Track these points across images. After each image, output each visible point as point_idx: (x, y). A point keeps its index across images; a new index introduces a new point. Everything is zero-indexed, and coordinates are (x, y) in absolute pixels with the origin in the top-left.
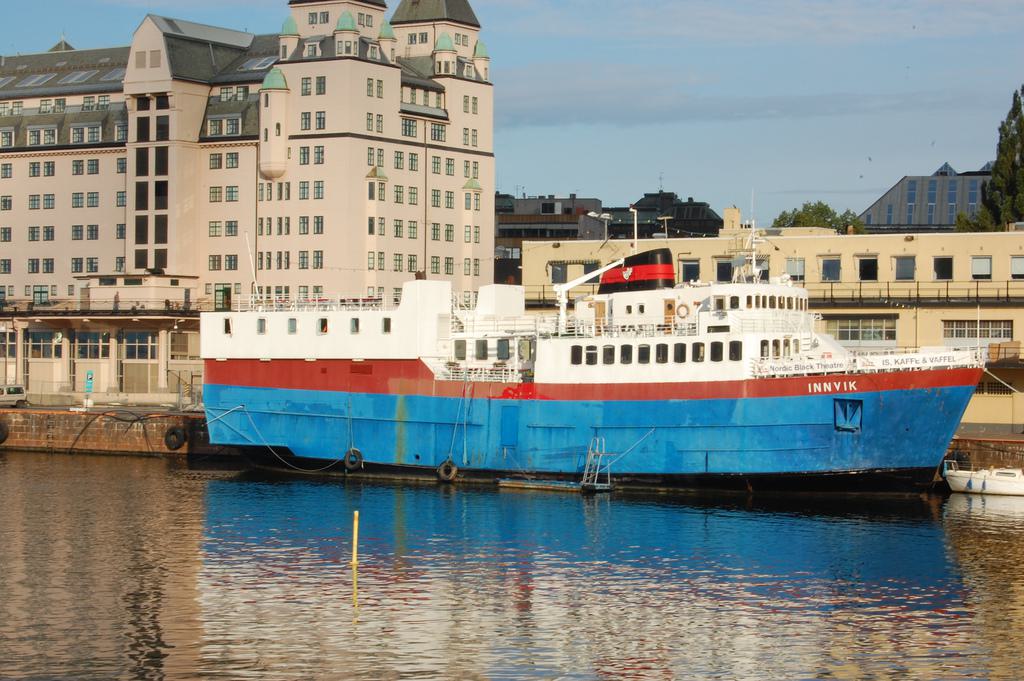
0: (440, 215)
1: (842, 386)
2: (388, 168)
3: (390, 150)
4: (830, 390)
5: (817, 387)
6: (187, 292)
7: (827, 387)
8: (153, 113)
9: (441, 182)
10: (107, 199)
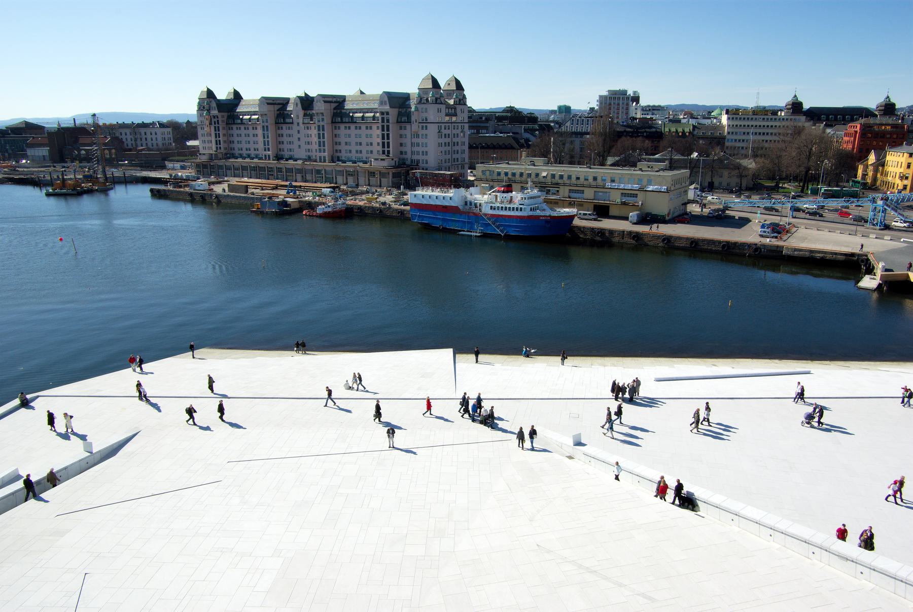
0: (455, 140)
2: (443, 130)
3: (443, 125)
8: (385, 116)
9: (455, 132)
10: (375, 136)
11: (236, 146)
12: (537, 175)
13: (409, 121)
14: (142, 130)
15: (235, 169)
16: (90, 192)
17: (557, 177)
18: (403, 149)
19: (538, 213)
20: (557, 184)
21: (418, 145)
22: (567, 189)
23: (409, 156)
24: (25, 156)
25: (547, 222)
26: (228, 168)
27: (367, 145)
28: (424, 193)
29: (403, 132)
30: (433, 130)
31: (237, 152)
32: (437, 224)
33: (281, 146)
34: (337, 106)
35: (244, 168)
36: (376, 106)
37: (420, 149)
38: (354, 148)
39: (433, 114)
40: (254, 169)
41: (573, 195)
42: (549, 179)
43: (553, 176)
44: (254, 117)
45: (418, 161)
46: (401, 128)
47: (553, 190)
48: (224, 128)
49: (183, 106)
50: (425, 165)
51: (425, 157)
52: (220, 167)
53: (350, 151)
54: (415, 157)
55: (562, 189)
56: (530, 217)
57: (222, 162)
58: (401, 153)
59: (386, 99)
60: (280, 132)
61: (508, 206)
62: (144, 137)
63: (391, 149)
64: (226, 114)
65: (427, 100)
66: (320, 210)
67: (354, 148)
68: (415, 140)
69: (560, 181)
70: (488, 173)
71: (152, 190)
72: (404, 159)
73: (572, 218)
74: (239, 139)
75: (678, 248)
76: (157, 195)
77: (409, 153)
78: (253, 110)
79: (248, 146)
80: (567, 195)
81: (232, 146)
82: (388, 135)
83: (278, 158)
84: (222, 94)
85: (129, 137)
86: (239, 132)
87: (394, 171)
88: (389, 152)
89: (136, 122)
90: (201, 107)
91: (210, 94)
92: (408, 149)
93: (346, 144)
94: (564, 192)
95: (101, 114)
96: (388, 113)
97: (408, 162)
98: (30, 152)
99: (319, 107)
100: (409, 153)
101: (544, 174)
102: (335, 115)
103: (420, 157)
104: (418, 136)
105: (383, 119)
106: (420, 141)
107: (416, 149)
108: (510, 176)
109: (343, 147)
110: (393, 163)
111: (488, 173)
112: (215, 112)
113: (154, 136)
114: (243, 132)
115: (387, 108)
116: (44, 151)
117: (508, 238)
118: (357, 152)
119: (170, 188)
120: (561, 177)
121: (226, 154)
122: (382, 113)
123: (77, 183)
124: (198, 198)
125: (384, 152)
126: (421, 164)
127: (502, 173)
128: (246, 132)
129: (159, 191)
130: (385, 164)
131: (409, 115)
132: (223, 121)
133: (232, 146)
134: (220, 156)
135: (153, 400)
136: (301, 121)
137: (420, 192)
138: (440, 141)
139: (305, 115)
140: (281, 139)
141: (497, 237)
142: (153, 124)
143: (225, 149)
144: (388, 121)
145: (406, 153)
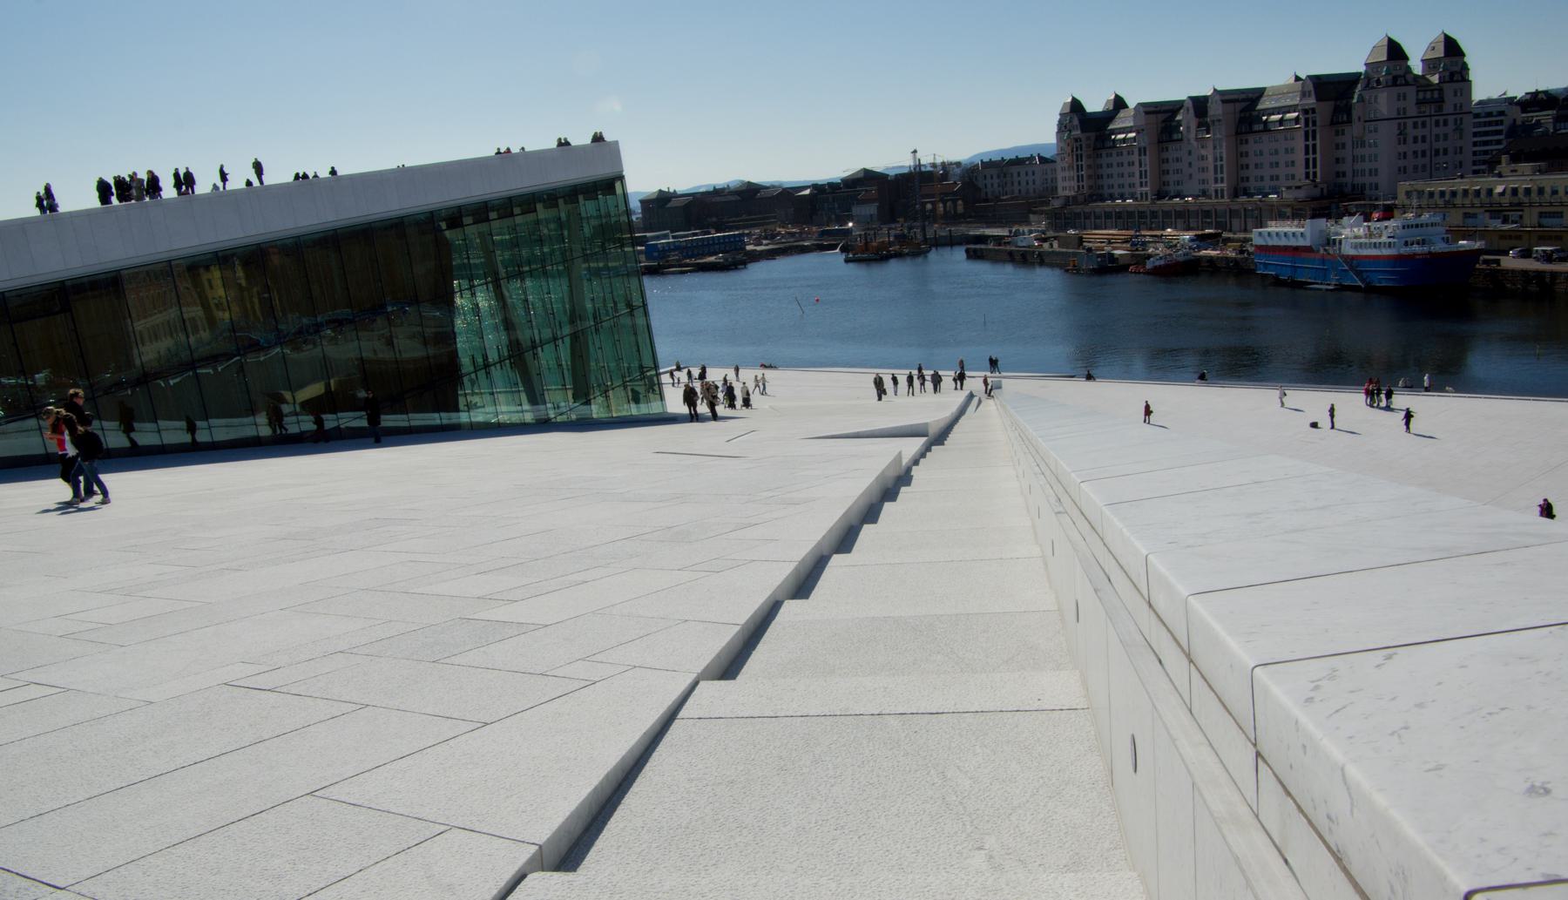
0: (1440, 145)
11: (1106, 182)
12: (1490, 192)
13: (1349, 121)
14: (1014, 170)
15: (1097, 217)
16: (899, 255)
17: (1521, 194)
18: (1341, 168)
19: (1416, 249)
20: (1519, 204)
21: (1363, 159)
22: (1536, 211)
23: (1348, 179)
24: (851, 218)
26: (1087, 216)
27: (1287, 163)
28: (1286, 229)
29: (1340, 139)
30: (1387, 132)
31: (1106, 191)
33: (1244, 173)
34: (1243, 110)
35: (1108, 215)
36: (1296, 101)
37: (1367, 166)
38: (1267, 172)
39: (1384, 103)
40: (1119, 215)
41: (1545, 221)
42: (1506, 200)
43: (1515, 191)
44: (1289, 116)
45: (1363, 186)
46: (1337, 133)
47: (1513, 215)
48: (1089, 157)
49: (1036, 131)
51: (1373, 180)
52: (1078, 215)
53: (1262, 178)
54: (1359, 180)
55: (1526, 214)
57: (1078, 209)
59: (1310, 87)
60: (1340, 139)
62: (1016, 179)
64: (1093, 135)
65: (1378, 82)
66: (1149, 265)
67: (1267, 172)
68: (1359, 151)
69: (1526, 200)
71: (967, 251)
74: (1109, 171)
76: (973, 255)
77: (1349, 174)
78: (1289, 102)
79: (1121, 181)
80: (1535, 221)
81: (1100, 182)
82: (1307, 153)
83: (1160, 195)
84: (1095, 104)
85: (996, 181)
86: (1109, 160)
89: (1007, 158)
90: (1063, 127)
91: (1076, 106)
92: (1347, 167)
93: (1424, 154)
94: (1531, 218)
96: (1313, 111)
97: (1348, 190)
98: (856, 210)
99: (1215, 110)
100: (1349, 174)
101: (1499, 189)
102: (1241, 121)
103: (1367, 180)
104: (1363, 144)
105: (1307, 121)
106: (1365, 151)
107: (1359, 166)
108: (1447, 197)
109: (1252, 173)
110: (1317, 192)
112: (1077, 133)
113: (1030, 178)
114: (1115, 159)
115: (1311, 101)
116: (871, 209)
117: (1370, 290)
119: (991, 246)
120: (1528, 191)
121: (1091, 196)
122: (1306, 112)
123: (883, 246)
124: (1018, 257)
125: (1307, 176)
126: (1367, 192)
127: (1521, 191)
128: (1119, 159)
129: (975, 251)
131: (1348, 110)
132: (1088, 146)
133: (1100, 182)
134: (1081, 199)
135: (284, 689)
136: (1192, 135)
137: (1274, 227)
138: (1402, 148)
139: (1200, 125)
140: (1165, 167)
142: (1032, 158)
143: (1090, 187)
144: (1314, 123)
145: (1344, 174)
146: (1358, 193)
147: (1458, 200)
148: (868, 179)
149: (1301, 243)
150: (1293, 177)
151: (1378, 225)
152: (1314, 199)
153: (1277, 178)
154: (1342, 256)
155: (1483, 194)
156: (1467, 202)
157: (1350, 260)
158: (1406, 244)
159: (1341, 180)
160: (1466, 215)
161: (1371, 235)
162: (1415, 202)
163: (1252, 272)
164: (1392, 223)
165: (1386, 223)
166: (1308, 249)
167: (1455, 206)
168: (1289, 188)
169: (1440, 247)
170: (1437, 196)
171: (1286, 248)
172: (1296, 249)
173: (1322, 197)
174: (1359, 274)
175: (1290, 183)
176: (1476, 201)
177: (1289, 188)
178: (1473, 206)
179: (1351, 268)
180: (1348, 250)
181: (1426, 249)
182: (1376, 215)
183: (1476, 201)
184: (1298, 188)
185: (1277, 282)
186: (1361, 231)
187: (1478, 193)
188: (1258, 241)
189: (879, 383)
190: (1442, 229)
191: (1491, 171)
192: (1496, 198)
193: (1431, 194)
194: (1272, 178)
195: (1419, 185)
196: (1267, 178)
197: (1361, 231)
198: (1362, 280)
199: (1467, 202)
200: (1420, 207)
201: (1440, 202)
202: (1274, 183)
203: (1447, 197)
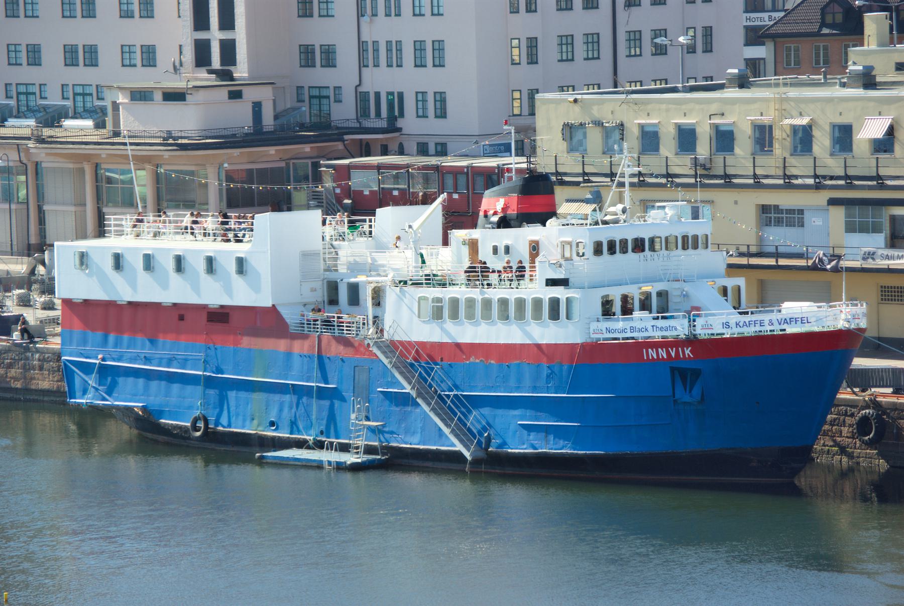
1: (677, 353)
4: (660, 350)
5: (652, 353)
6: (257, 107)
7: (663, 353)
12: (843, 136)
19: (642, 326)
23: (344, 75)
25: (683, 375)
32: (182, 411)
45: (397, 102)
50: (432, 127)
51: (429, 80)
53: (34, 56)
54: (381, 80)
56: (591, 354)
58: (307, 56)
61: (512, 294)
63: (240, 34)
70: (594, 138)
72: (319, 96)
73: (839, 343)
75: (267, 463)
77: (347, 56)
87: (237, 159)
88: (228, 50)
95: (734, 87)
97: (344, 112)
100: (347, 56)
103: (406, 80)
108: (703, 150)
110: (239, 117)
111: (594, 138)
117: (497, 466)
118: (71, 56)
125: (202, 56)
126: (410, 123)
130: (186, 120)
141: (447, 463)
145: (329, 57)
146: (379, 125)
147: (741, 159)
148: (205, 307)
149: (241, 295)
150: (149, 56)
151: (507, 236)
152: (231, 141)
153: (92, 56)
154: (392, 347)
155: (822, 142)
156: (769, 165)
157: (421, 360)
158: (607, 309)
159: (320, 76)
160: (769, 215)
161: (478, 273)
162: (627, 167)
163: (56, 401)
164: (549, 234)
165: (532, 232)
166: (265, 322)
167: (728, 181)
168: (140, 96)
169: (721, 321)
170: (668, 147)
171: (181, 314)
172: (220, 317)
173: (257, 137)
174: (455, 409)
175: (142, 78)
176: (800, 167)
177: (140, 96)
178: (789, 183)
179: (426, 390)
180: (407, 321)
181: (679, 328)
182: (494, 202)
183: (800, 167)
184: (175, 96)
185: (152, 435)
186: (449, 259)
187: (803, 139)
188: (72, 284)
189: (442, 114)
190: (717, 260)
191: (830, 65)
192: (862, 159)
193: (650, 140)
194: (71, 56)
195: (611, 108)
196: (53, 56)
197: (449, 259)
198: (463, 433)
199: (769, 165)
200: (641, 182)
201: (682, 165)
202: (81, 75)
203: (703, 150)
